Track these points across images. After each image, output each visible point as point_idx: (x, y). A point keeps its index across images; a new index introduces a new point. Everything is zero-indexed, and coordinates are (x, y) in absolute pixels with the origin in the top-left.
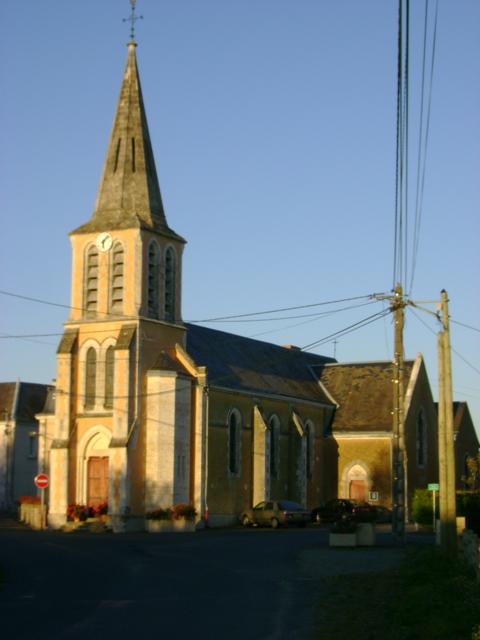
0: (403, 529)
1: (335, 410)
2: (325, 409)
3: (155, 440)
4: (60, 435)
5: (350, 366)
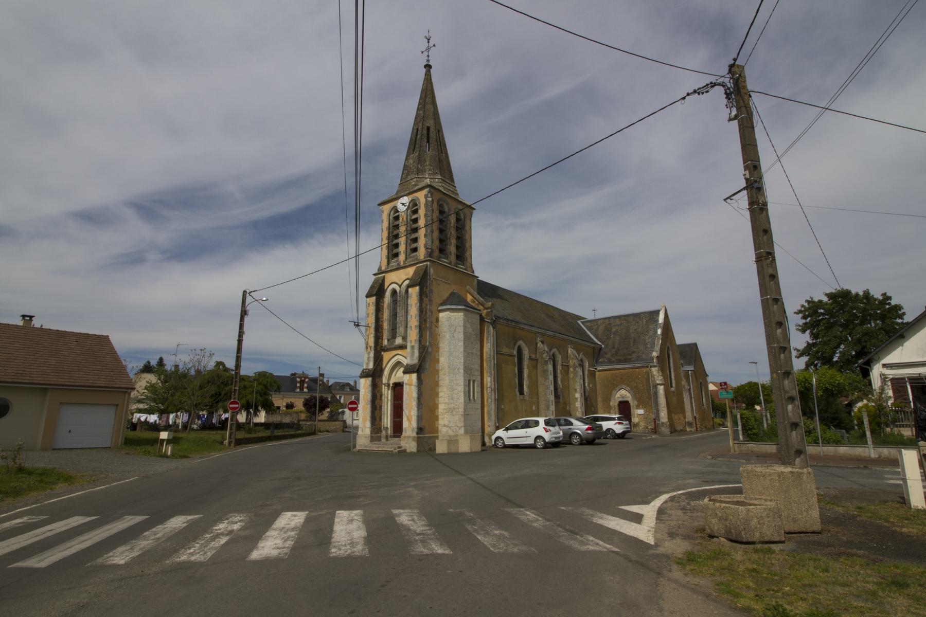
0: (343, 406)
1: (601, 349)
2: (594, 348)
3: (446, 365)
4: (368, 364)
5: (610, 318)
